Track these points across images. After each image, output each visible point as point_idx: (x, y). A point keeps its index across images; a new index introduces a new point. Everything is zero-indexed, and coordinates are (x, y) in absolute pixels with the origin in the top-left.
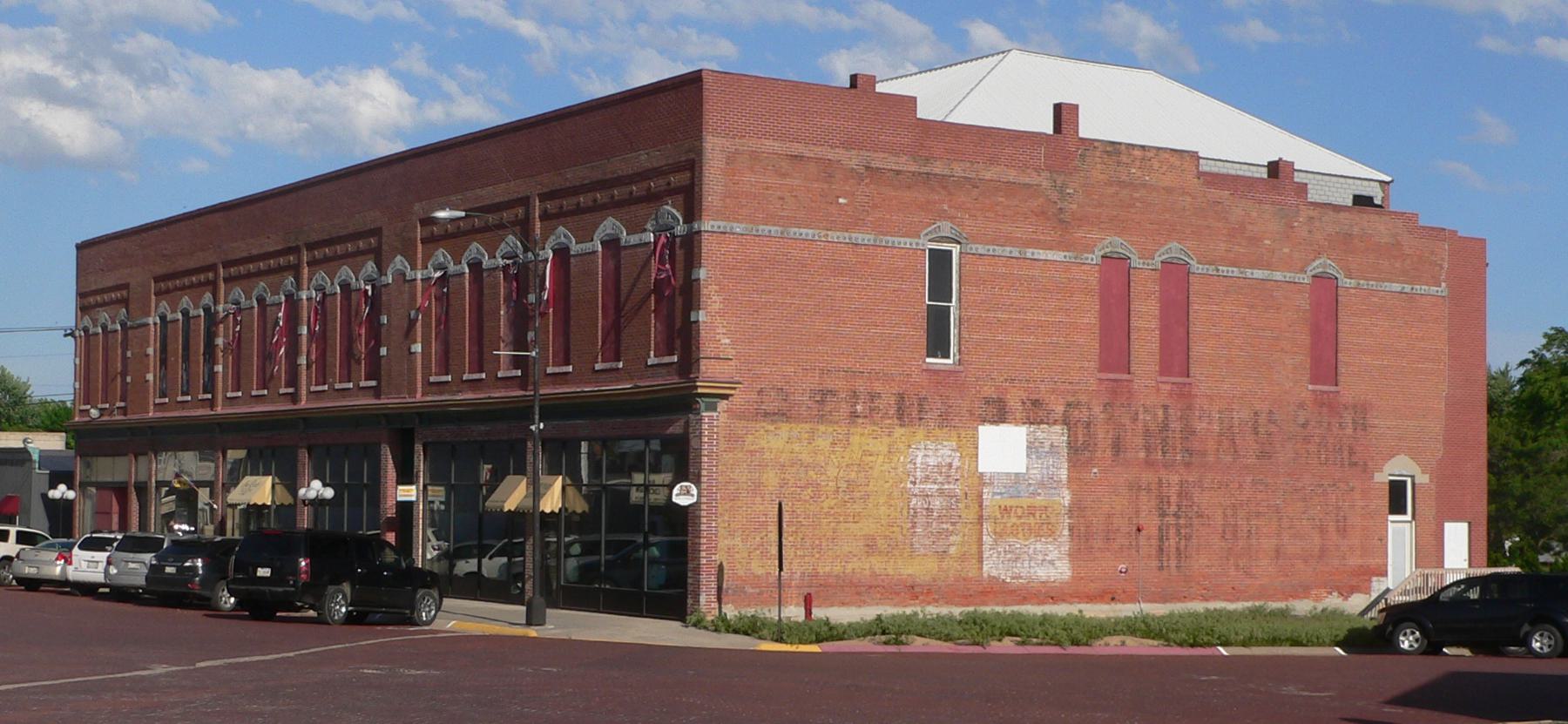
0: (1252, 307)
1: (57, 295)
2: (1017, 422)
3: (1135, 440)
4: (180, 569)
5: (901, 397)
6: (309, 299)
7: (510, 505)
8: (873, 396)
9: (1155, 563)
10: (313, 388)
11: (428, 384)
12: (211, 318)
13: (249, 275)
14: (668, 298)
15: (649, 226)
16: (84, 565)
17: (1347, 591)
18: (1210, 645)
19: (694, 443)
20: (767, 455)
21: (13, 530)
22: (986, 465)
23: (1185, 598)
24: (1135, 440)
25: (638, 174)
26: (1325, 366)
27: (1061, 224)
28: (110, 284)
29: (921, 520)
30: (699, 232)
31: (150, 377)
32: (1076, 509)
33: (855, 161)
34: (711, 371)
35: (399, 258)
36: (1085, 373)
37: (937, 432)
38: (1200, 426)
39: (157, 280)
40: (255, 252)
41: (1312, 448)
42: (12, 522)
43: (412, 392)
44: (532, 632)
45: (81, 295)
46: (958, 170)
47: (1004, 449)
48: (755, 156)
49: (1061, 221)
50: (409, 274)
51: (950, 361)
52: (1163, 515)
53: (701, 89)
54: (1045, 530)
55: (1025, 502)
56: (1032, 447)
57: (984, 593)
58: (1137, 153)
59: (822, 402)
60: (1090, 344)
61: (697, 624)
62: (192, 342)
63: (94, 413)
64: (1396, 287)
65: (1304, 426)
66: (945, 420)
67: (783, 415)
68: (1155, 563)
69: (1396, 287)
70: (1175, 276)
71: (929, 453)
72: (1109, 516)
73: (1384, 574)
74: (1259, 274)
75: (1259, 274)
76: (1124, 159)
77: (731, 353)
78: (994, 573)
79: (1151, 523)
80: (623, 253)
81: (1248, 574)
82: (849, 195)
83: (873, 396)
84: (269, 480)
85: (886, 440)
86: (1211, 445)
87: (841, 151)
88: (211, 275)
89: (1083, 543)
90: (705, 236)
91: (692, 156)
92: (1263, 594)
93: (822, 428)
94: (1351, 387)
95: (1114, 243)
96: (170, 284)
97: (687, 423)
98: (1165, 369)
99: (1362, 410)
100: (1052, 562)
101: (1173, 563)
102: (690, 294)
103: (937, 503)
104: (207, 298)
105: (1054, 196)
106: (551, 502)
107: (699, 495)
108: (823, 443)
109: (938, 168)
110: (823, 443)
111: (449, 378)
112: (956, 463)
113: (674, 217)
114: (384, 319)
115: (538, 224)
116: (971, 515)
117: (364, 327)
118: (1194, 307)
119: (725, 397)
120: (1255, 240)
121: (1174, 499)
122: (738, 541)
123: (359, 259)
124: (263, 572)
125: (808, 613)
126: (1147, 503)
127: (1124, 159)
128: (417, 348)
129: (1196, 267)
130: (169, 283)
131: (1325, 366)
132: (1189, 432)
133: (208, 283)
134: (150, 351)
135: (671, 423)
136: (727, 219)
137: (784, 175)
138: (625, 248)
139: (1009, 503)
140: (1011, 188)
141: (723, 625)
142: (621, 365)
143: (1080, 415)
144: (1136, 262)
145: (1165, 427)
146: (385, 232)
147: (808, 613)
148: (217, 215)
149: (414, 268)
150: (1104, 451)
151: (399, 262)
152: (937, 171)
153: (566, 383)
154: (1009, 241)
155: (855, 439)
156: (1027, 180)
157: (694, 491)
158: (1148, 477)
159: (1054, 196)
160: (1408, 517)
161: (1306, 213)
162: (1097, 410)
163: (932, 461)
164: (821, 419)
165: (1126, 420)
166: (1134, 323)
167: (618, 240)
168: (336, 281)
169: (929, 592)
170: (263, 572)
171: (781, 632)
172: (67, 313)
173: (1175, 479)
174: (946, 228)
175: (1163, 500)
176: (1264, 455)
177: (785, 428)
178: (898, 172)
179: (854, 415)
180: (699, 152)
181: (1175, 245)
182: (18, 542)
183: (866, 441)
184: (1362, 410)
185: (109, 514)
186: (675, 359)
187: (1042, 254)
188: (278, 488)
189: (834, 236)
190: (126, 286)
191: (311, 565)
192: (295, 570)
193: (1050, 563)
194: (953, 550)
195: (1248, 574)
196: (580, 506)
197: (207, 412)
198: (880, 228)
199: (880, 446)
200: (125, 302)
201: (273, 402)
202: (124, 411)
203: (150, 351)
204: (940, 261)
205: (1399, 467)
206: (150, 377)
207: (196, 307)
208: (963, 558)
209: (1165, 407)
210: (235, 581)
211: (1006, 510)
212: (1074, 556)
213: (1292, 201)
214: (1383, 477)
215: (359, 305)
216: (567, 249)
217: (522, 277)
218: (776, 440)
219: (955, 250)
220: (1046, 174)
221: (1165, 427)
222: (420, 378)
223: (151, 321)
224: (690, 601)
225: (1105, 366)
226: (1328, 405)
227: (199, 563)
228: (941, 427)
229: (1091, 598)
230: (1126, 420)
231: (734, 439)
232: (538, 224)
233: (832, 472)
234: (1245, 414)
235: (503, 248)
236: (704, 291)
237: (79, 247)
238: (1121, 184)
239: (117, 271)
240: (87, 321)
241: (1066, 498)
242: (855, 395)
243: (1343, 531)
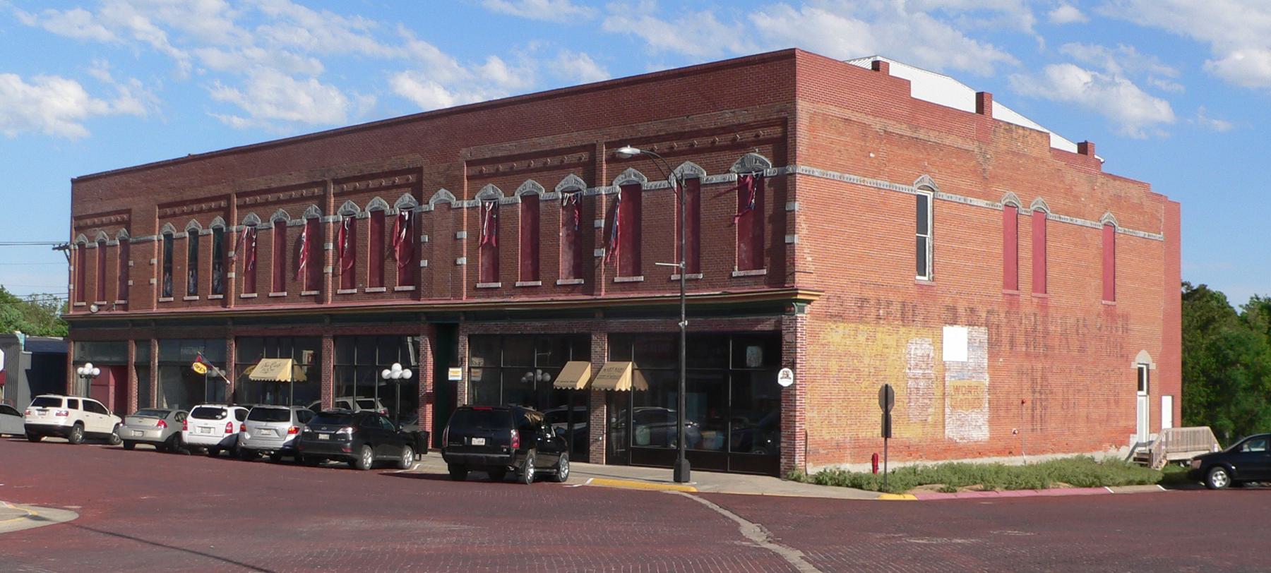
0: (1076, 245)
1: (57, 221)
2: (963, 324)
3: (1021, 339)
4: (334, 437)
5: (904, 304)
6: (240, 232)
7: (581, 385)
8: (889, 303)
9: (1030, 427)
10: (161, 299)
11: (474, 291)
12: (222, 239)
13: (266, 203)
14: (766, 220)
15: (733, 169)
16: (198, 430)
17: (1119, 444)
18: (1101, 486)
19: (787, 338)
20: (832, 348)
21: (65, 400)
22: (947, 357)
23: (1043, 452)
24: (1021, 339)
25: (723, 128)
26: (1110, 291)
27: (985, 181)
28: (110, 209)
29: (913, 396)
30: (794, 174)
31: (154, 281)
32: (992, 388)
33: (878, 127)
34: (801, 280)
35: (443, 190)
36: (996, 290)
37: (922, 331)
38: (1052, 328)
39: (161, 206)
40: (274, 185)
41: (1104, 345)
42: (65, 395)
43: (457, 295)
44: (676, 489)
45: (76, 218)
46: (933, 137)
47: (958, 344)
48: (825, 118)
49: (985, 178)
50: (454, 203)
51: (926, 278)
52: (1034, 392)
53: (794, 64)
54: (975, 404)
55: (967, 383)
56: (971, 342)
57: (945, 450)
58: (1021, 131)
59: (861, 307)
60: (998, 267)
61: (797, 479)
62: (200, 255)
63: (94, 308)
64: (1141, 234)
65: (1100, 329)
66: (926, 321)
67: (839, 317)
68: (1030, 427)
69: (1141, 234)
70: (1040, 219)
71: (918, 347)
72: (1008, 393)
73: (1135, 433)
74: (1080, 221)
75: (1080, 221)
76: (1014, 135)
77: (811, 268)
78: (951, 435)
79: (1028, 397)
80: (702, 189)
81: (1075, 434)
82: (876, 151)
83: (889, 303)
84: (290, 362)
85: (895, 336)
86: (1056, 342)
87: (871, 117)
88: (223, 203)
89: (997, 414)
90: (798, 176)
91: (783, 115)
92: (1081, 449)
93: (861, 327)
94: (1122, 304)
95: (1010, 196)
96: (177, 210)
97: (779, 322)
98: (1035, 290)
99: (1126, 317)
100: (980, 427)
101: (1039, 427)
102: (784, 222)
103: (922, 384)
104: (219, 221)
105: (981, 160)
106: (624, 384)
107: (795, 379)
108: (861, 338)
109: (922, 134)
110: (861, 338)
111: (500, 285)
112: (932, 355)
113: (763, 162)
114: (425, 238)
115: (605, 166)
116: (938, 393)
117: (406, 249)
118: (1049, 243)
119: (809, 302)
120: (1077, 198)
121: (1039, 381)
122: (815, 414)
123: (394, 191)
124: (477, 442)
125: (875, 468)
126: (1027, 384)
127: (1014, 135)
128: (463, 261)
129: (1051, 216)
130: (173, 209)
131: (1110, 291)
132: (1046, 333)
133: (219, 209)
134: (155, 261)
135: (758, 322)
136: (810, 165)
137: (841, 134)
138: (706, 185)
139: (959, 383)
140: (960, 152)
141: (819, 481)
142: (701, 276)
143: (994, 319)
144: (1022, 210)
145: (1035, 330)
146: (426, 170)
147: (875, 468)
148: (231, 158)
149: (460, 198)
150: (1006, 347)
151: (443, 194)
152: (921, 136)
153: (537, 294)
154: (956, 190)
155: (879, 335)
156: (967, 147)
157: (791, 375)
158: (1027, 365)
159: (981, 160)
160: (1144, 393)
161: (1101, 179)
162: (1003, 315)
163: (919, 353)
164: (861, 319)
165: (1016, 324)
166: (1020, 254)
167: (698, 179)
168: (368, 209)
169: (918, 450)
170: (477, 442)
171: (856, 483)
172: (63, 233)
173: (1040, 366)
174: (926, 179)
175: (1033, 380)
176: (1082, 350)
177: (841, 325)
178: (902, 136)
179: (878, 318)
180: (794, 112)
181: (1039, 199)
182: (85, 409)
183: (885, 336)
184: (1126, 317)
185: (107, 386)
186: (765, 272)
187: (976, 202)
188: (637, 372)
189: (869, 181)
190: (129, 211)
191: (521, 435)
192: (508, 441)
193: (973, 427)
194: (930, 419)
195: (1075, 434)
196: (643, 386)
197: (219, 308)
198: (892, 178)
199: (891, 341)
200: (127, 224)
201: (293, 302)
202: (125, 307)
203: (155, 261)
204: (922, 201)
205: (1143, 358)
206: (154, 281)
207: (206, 227)
208: (935, 425)
209: (1035, 315)
210: (449, 449)
211: (957, 389)
212: (992, 422)
213: (1094, 171)
214: (1135, 366)
215: (394, 226)
216: (638, 186)
217: (583, 208)
218: (837, 335)
219: (930, 195)
220: (976, 143)
221: (1035, 330)
222: (462, 282)
223: (155, 238)
224: (783, 461)
225: (1006, 286)
226: (1110, 313)
227: (350, 430)
228: (924, 327)
229: (999, 453)
230: (1016, 324)
231: (814, 334)
232: (605, 166)
233: (867, 360)
234: (1071, 321)
235: (563, 184)
236: (797, 220)
237: (73, 181)
238: (1014, 153)
239: (106, 205)
240: (82, 237)
241: (986, 379)
242: (879, 302)
243: (1117, 402)
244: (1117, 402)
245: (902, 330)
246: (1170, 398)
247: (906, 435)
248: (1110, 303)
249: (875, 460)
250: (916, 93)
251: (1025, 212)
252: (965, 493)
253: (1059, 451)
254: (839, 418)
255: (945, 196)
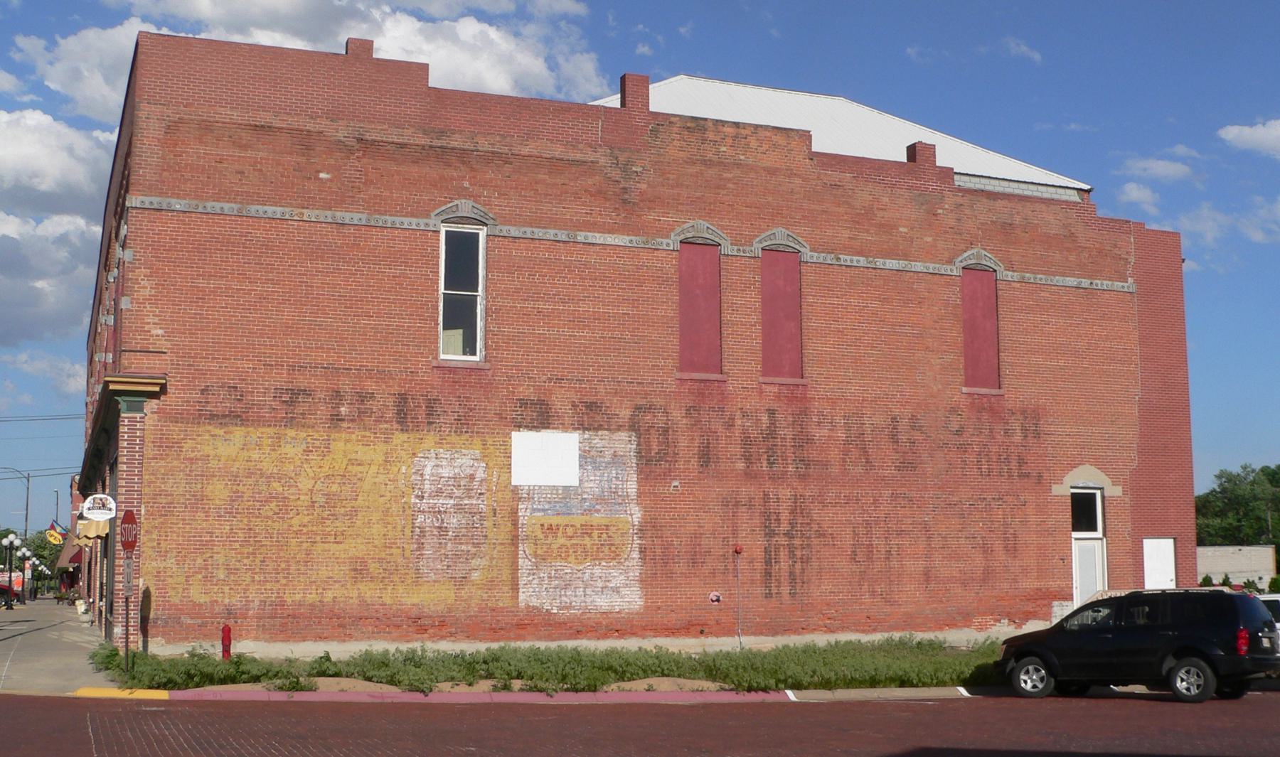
2: (565, 428)
20: (213, 464)
27: (626, 207)
32: (649, 527)
36: (660, 370)
38: (819, 433)
49: (625, 202)
51: (476, 358)
64: (1071, 281)
68: (760, 590)
70: (782, 263)
78: (535, 602)
85: (382, 447)
89: (659, 565)
94: (1018, 390)
99: (1033, 417)
112: (480, 474)
121: (785, 516)
137: (244, 147)
145: (771, 433)
183: (348, 446)
184: (1033, 417)
194: (475, 576)
199: (376, 453)
205: (1084, 478)
208: (490, 584)
209: (771, 412)
212: (646, 582)
218: (227, 446)
221: (771, 433)
225: (686, 364)
228: (458, 432)
229: (672, 631)
233: (305, 484)
238: (708, 163)
242: (337, 395)
244: (1012, 550)
245: (399, 438)
246: (1167, 545)
247: (415, 600)
248: (994, 392)
249: (226, 638)
250: (435, 81)
251: (740, 250)
252: (518, 694)
253: (843, 629)
254: (230, 571)
255: (506, 230)
